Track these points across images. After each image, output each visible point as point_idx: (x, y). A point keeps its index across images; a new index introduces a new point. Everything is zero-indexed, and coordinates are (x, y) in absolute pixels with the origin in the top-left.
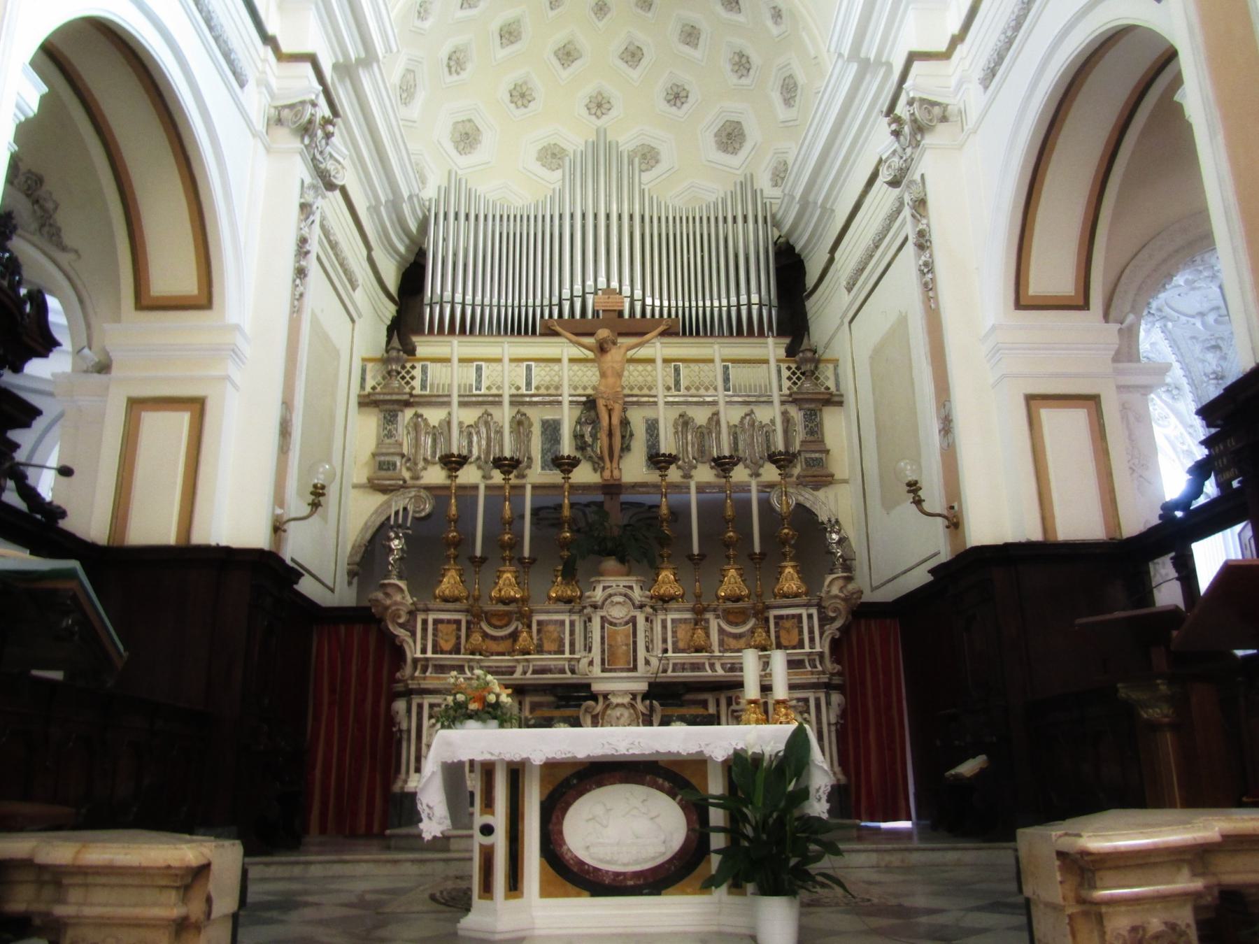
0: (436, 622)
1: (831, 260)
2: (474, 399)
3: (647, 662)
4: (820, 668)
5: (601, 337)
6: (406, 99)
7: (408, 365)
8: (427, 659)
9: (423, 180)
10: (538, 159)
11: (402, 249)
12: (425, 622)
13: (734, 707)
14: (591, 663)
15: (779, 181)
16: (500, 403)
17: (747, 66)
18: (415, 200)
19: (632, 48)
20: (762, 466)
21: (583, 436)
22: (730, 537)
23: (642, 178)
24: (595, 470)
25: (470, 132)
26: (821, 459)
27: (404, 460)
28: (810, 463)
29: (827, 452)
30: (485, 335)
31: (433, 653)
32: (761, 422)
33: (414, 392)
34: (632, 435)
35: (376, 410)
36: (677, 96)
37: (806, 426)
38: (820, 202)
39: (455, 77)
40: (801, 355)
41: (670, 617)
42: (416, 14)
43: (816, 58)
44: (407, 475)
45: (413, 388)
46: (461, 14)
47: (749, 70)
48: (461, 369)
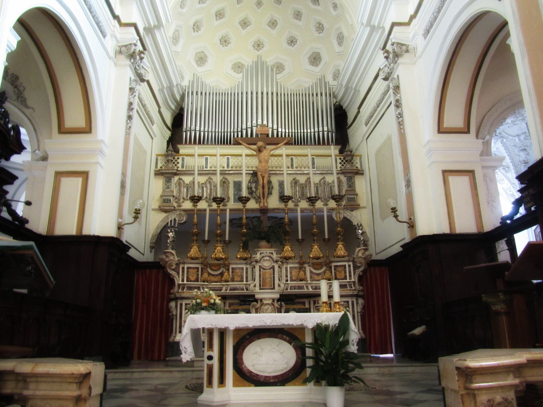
0: (188, 268)
1: (358, 112)
2: (204, 172)
3: (279, 286)
4: (354, 288)
5: (259, 145)
6: (175, 43)
7: (176, 158)
8: (184, 284)
9: (182, 78)
10: (232, 69)
11: (173, 107)
12: (183, 268)
13: (317, 305)
14: (255, 286)
15: (336, 78)
16: (216, 174)
17: (322, 28)
18: (179, 86)
19: (272, 21)
20: (329, 201)
21: (251, 188)
22: (315, 232)
23: (277, 77)
24: (257, 203)
25: (203, 57)
26: (354, 198)
27: (174, 198)
28: (349, 200)
29: (357, 195)
30: (209, 145)
31: (187, 282)
32: (328, 182)
33: (179, 169)
34: (272, 188)
35: (162, 177)
36: (292, 42)
37: (348, 184)
38: (353, 87)
39: (196, 33)
40: (345, 153)
41: (289, 266)
42: (180, 6)
43: (352, 25)
44: (175, 205)
45: (178, 167)
46: (199, 6)
47: (323, 30)
48: (199, 159)
